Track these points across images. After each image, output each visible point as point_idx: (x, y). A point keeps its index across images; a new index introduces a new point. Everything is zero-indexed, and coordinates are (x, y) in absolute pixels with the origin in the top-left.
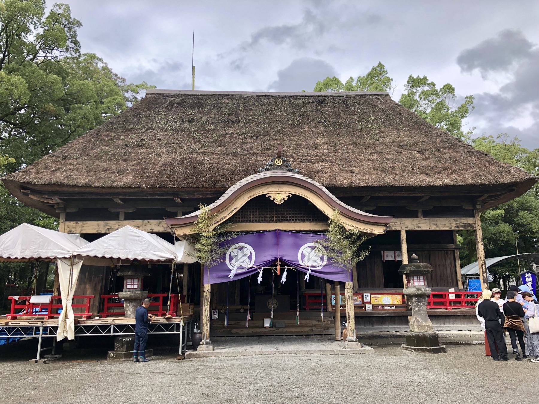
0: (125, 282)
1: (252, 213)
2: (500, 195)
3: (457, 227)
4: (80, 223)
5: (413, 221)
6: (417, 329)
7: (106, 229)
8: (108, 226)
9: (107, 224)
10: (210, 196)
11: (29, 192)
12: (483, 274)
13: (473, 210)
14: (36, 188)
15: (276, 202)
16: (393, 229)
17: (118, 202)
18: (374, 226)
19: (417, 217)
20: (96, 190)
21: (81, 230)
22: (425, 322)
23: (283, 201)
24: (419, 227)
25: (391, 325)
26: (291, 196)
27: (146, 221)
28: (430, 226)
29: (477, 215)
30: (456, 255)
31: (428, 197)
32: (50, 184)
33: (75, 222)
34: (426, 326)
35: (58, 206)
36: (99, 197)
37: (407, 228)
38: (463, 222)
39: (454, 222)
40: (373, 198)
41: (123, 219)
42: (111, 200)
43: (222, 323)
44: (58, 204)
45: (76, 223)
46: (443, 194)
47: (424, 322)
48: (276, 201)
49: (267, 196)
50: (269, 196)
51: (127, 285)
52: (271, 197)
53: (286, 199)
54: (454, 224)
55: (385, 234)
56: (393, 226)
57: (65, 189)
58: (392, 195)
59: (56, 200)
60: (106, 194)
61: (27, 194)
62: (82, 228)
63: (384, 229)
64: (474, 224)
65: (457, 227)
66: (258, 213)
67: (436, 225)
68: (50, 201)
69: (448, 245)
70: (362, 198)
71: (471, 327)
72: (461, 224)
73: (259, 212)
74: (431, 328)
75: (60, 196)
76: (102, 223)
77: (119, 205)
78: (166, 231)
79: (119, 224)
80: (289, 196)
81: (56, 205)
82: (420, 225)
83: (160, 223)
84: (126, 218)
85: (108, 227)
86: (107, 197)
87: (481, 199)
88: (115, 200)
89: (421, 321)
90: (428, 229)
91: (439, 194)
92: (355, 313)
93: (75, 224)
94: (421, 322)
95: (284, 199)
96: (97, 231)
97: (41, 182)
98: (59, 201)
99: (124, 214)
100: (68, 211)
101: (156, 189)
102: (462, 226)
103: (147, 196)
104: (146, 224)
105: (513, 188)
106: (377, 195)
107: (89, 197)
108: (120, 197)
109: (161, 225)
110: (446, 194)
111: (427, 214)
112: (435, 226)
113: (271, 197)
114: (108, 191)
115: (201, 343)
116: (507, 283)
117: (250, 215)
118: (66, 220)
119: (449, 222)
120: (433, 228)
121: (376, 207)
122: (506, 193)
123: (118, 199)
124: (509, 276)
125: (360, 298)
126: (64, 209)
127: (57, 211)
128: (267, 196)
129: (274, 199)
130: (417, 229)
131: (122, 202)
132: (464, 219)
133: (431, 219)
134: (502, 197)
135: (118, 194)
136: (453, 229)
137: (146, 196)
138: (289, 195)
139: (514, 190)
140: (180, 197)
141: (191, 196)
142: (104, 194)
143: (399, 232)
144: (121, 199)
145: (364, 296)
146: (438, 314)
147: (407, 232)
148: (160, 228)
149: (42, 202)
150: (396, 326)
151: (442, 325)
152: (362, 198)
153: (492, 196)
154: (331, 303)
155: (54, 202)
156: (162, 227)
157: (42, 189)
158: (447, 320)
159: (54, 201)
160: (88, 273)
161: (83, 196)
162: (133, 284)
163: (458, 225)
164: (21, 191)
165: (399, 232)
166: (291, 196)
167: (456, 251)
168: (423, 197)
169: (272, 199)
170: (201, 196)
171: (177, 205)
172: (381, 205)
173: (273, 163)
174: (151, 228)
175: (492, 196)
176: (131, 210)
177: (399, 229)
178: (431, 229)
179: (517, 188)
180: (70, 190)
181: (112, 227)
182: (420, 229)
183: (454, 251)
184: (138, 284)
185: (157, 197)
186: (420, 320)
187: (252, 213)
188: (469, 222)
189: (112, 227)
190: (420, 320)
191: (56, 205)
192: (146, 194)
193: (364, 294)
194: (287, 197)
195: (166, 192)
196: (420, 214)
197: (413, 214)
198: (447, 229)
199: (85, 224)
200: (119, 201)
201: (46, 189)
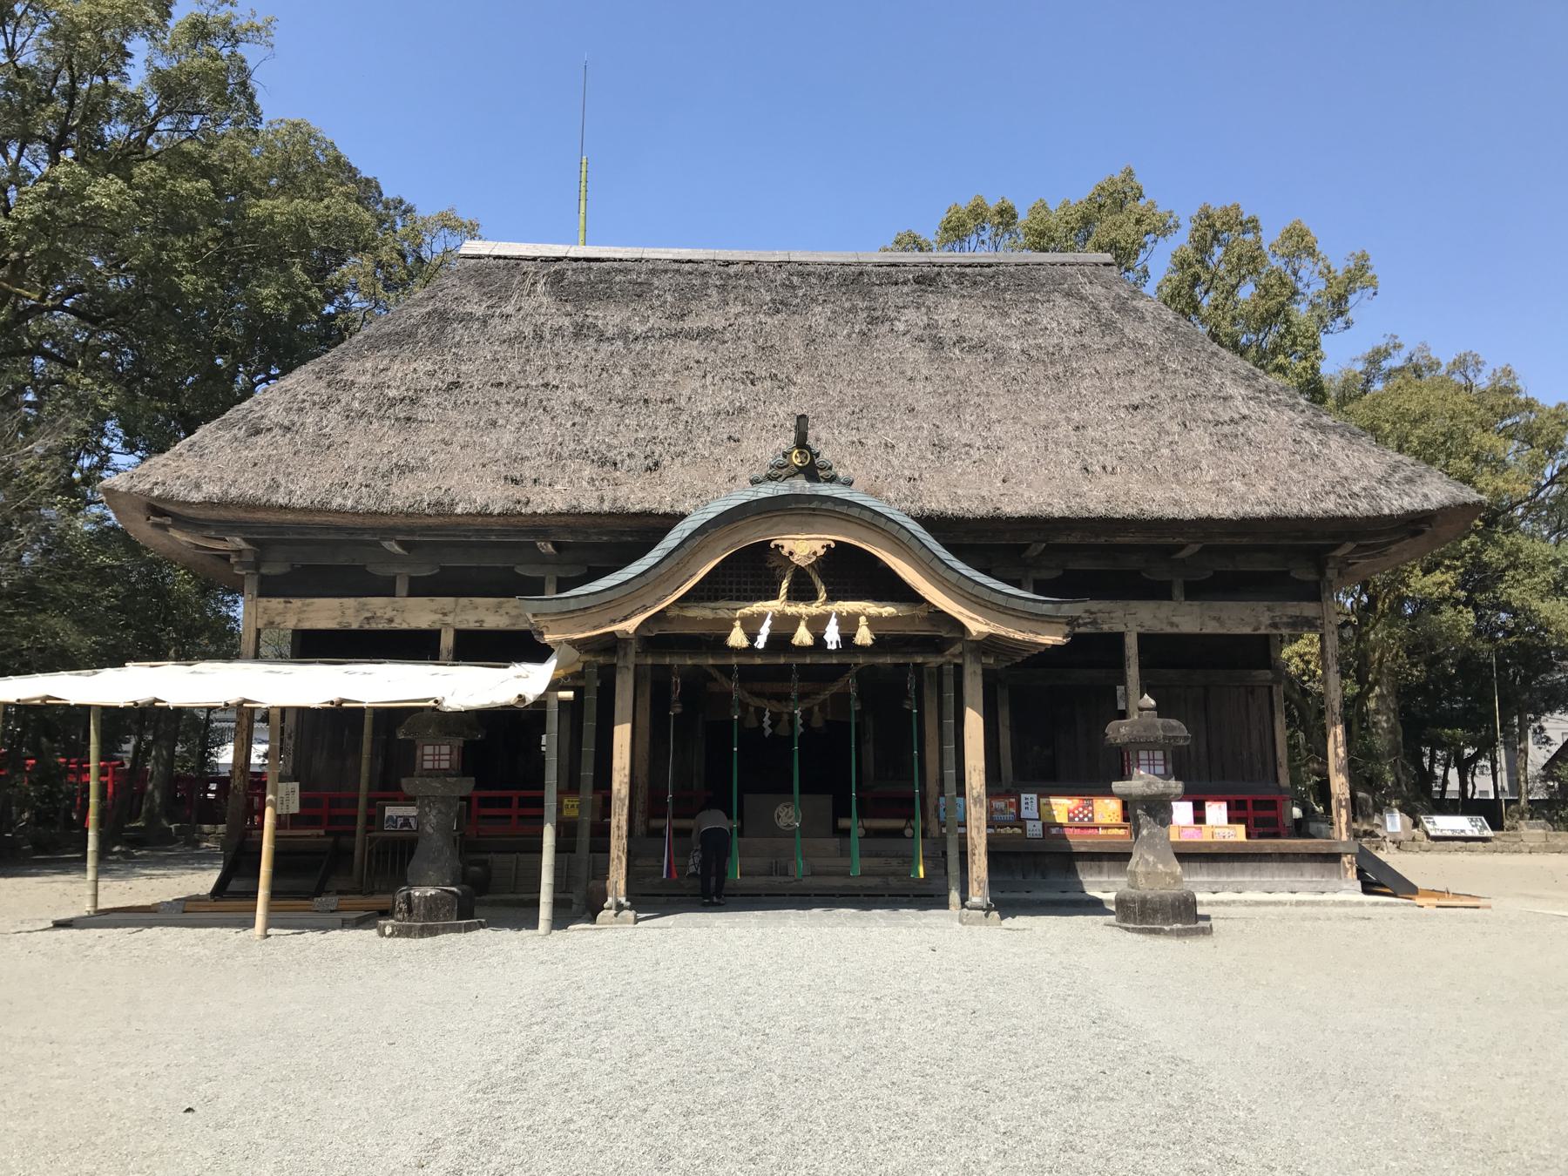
0: (419, 753)
1: (734, 587)
2: (1390, 543)
3: (1274, 625)
4: (297, 603)
5: (1159, 608)
6: (1143, 881)
7: (362, 618)
8: (368, 610)
9: (365, 604)
10: (630, 539)
11: (168, 521)
12: (1336, 748)
13: (1317, 583)
14: (190, 512)
15: (794, 559)
16: (1106, 628)
17: (392, 550)
18: (1040, 624)
19: (1169, 597)
20: (338, 520)
21: (299, 621)
22: (1165, 865)
23: (814, 558)
24: (1172, 624)
25: (1091, 876)
26: (833, 545)
27: (464, 601)
28: (1202, 624)
29: (1327, 594)
30: (1275, 699)
31: (1197, 547)
32: (223, 504)
33: (282, 600)
34: (1167, 874)
35: (239, 557)
36: (343, 537)
37: (1142, 627)
38: (1289, 613)
39: (1267, 614)
40: (1052, 549)
41: (405, 594)
42: (377, 544)
43: (659, 861)
44: (239, 552)
45: (286, 602)
46: (1237, 541)
47: (1160, 866)
48: (796, 557)
49: (772, 545)
50: (777, 546)
51: (423, 760)
52: (782, 547)
53: (821, 552)
54: (1265, 619)
55: (1067, 644)
56: (1104, 622)
57: (260, 515)
58: (1102, 540)
59: (237, 542)
60: (364, 530)
61: (164, 527)
62: (302, 616)
63: (1067, 632)
64: (1319, 618)
65: (1274, 625)
66: (749, 587)
67: (1218, 619)
68: (220, 546)
69: (1255, 673)
70: (1026, 547)
71: (1296, 884)
72: (1285, 620)
73: (752, 583)
74: (1178, 880)
75: (246, 533)
76: (350, 602)
77: (395, 555)
78: (517, 628)
79: (395, 605)
80: (828, 546)
81: (233, 555)
82: (1175, 619)
83: (499, 606)
84: (411, 594)
85: (369, 615)
86: (367, 537)
87: (1339, 553)
88: (386, 544)
89: (1155, 864)
90: (1196, 630)
91: (1227, 541)
92: (989, 843)
93: (282, 606)
94: (1155, 864)
95: (815, 553)
96: (339, 623)
97: (196, 497)
98: (244, 545)
99: (407, 582)
100: (264, 571)
101: (492, 520)
102: (1287, 625)
103: (469, 537)
104: (465, 606)
105: (1423, 526)
106: (1062, 540)
107: (320, 537)
108: (399, 538)
109: (502, 611)
110: (1245, 541)
111: (1195, 591)
112: (1214, 623)
113: (782, 547)
114: (369, 522)
115: (606, 905)
116: (1469, 780)
117: (731, 591)
118: (260, 595)
119: (1254, 613)
120: (1211, 628)
121: (1061, 573)
122: (1403, 539)
123: (393, 543)
124: (1474, 759)
125: (1011, 805)
126: (256, 565)
127: (237, 571)
128: (772, 545)
129: (791, 553)
130: (1169, 630)
131: (404, 549)
132: (1292, 606)
133: (1206, 604)
134: (1394, 548)
135: (390, 532)
136: (1262, 631)
137: (465, 536)
138: (829, 542)
139: (1422, 532)
140: (552, 539)
141: (580, 539)
142: (359, 529)
143: (1120, 637)
144: (400, 543)
145: (1023, 801)
146: (217, 541)
147: (1141, 637)
148: (498, 618)
149: (198, 547)
150: (1104, 879)
151: (1224, 879)
152: (1026, 547)
153: (1367, 547)
154: (938, 817)
155: (230, 546)
156: (506, 617)
157: (202, 514)
158: (1236, 865)
159: (230, 545)
160: (46, 736)
161: (303, 534)
162: (439, 760)
163: (1277, 620)
164: (148, 519)
165: (1120, 637)
166: (833, 545)
167: (1275, 688)
168: (1181, 547)
169: (785, 552)
170: (605, 538)
171: (543, 560)
172: (1072, 566)
173: (786, 461)
174: (476, 619)
175: (1367, 547)
176: (425, 572)
177: (1120, 628)
178: (1204, 631)
179: (1431, 526)
180: (272, 517)
181: (379, 614)
182: (1175, 630)
183: (1270, 688)
184: (449, 760)
185: (493, 538)
186: (1151, 859)
187: (734, 587)
188: (1306, 614)
189: (379, 614)
190: (1151, 859)
191: (233, 555)
192: (464, 531)
193: (1023, 796)
194: (823, 547)
195: (517, 526)
196: (1177, 591)
197: (1158, 592)
198: (1248, 630)
199: (308, 605)
200: (397, 548)
201: (214, 514)
